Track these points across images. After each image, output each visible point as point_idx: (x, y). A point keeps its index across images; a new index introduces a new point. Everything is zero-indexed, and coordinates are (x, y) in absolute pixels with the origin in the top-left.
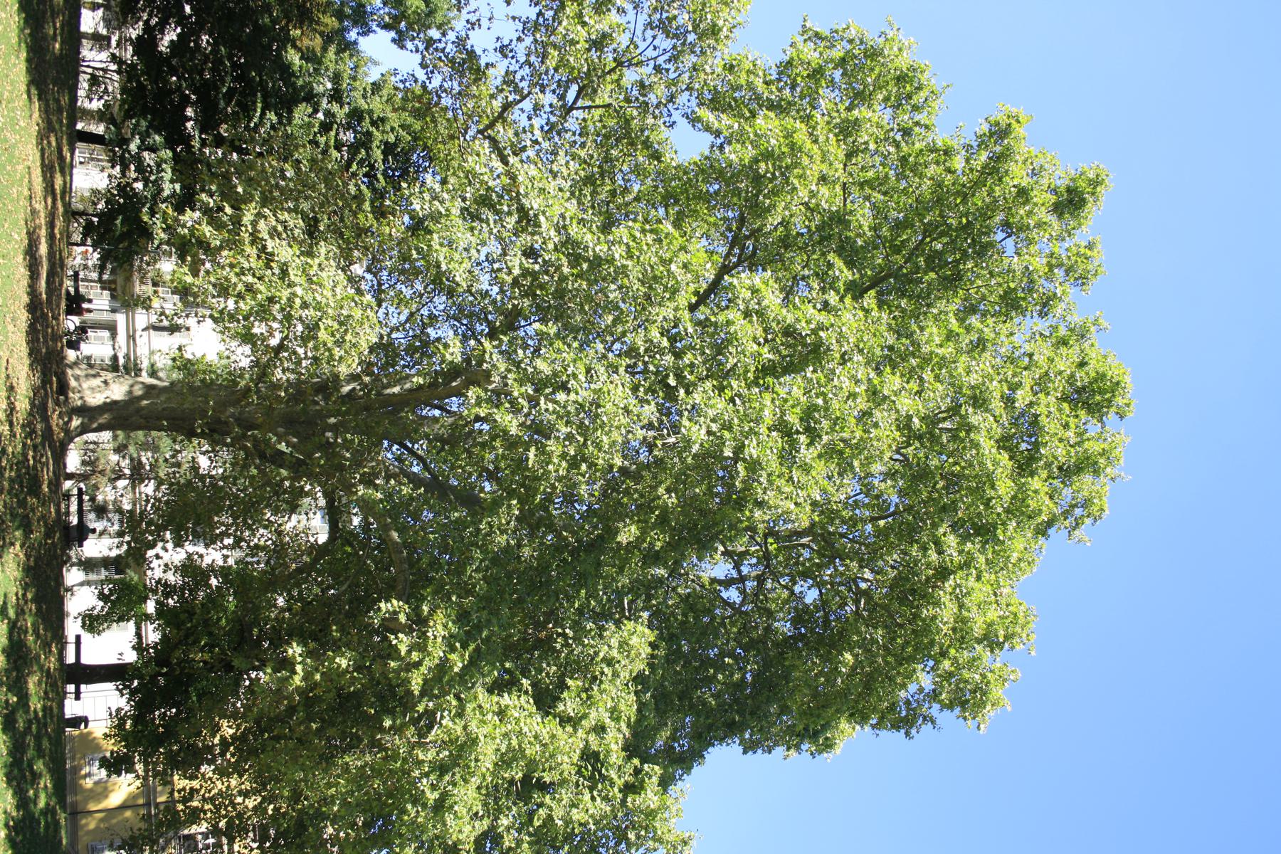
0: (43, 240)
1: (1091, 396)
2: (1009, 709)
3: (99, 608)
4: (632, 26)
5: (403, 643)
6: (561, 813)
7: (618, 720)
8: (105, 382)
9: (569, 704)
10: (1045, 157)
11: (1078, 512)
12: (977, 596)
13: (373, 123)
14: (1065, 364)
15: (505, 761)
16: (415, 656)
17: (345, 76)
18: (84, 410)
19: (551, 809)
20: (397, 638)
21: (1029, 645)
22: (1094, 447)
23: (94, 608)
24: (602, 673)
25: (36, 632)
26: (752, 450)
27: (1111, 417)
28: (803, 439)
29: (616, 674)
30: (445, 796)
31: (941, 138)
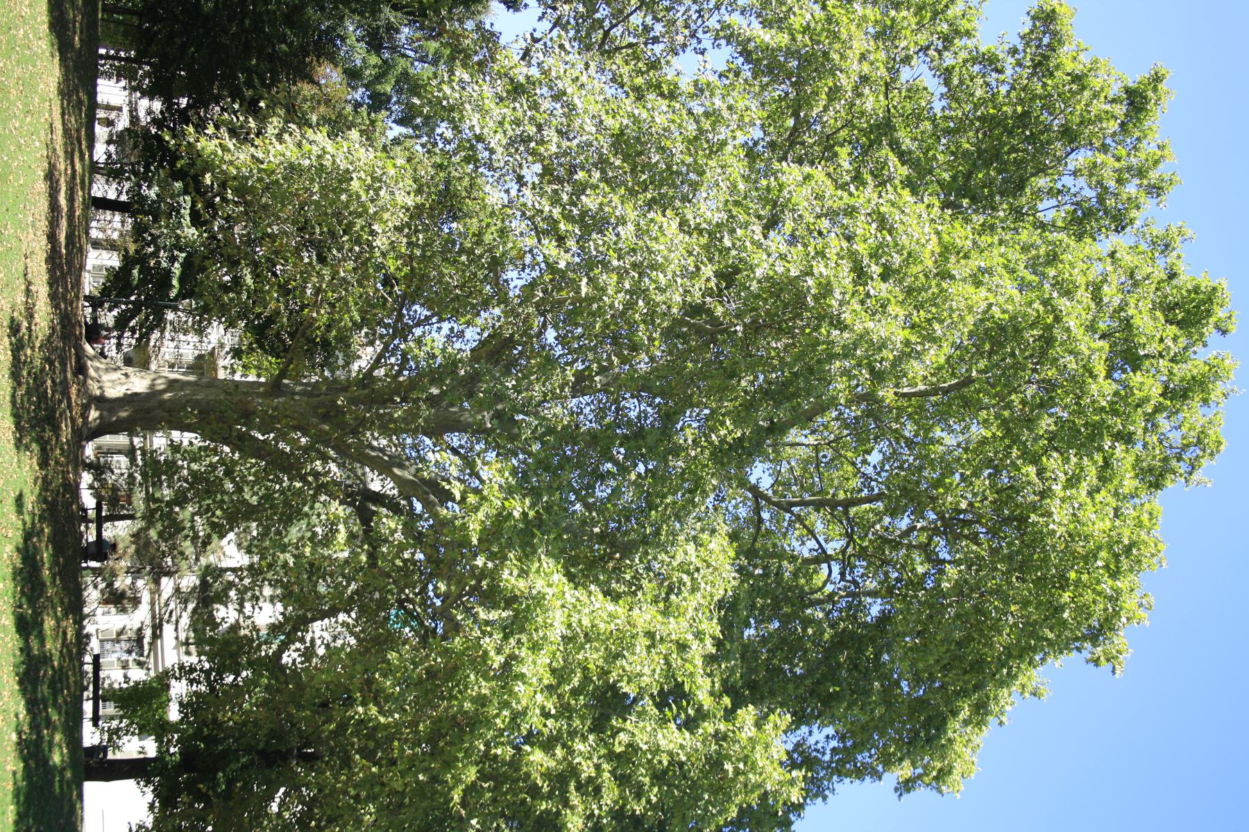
1: (1191, 313)
8: (126, 375)
10: (1104, 51)
18: (101, 401)
27: (1209, 331)
31: (985, 41)
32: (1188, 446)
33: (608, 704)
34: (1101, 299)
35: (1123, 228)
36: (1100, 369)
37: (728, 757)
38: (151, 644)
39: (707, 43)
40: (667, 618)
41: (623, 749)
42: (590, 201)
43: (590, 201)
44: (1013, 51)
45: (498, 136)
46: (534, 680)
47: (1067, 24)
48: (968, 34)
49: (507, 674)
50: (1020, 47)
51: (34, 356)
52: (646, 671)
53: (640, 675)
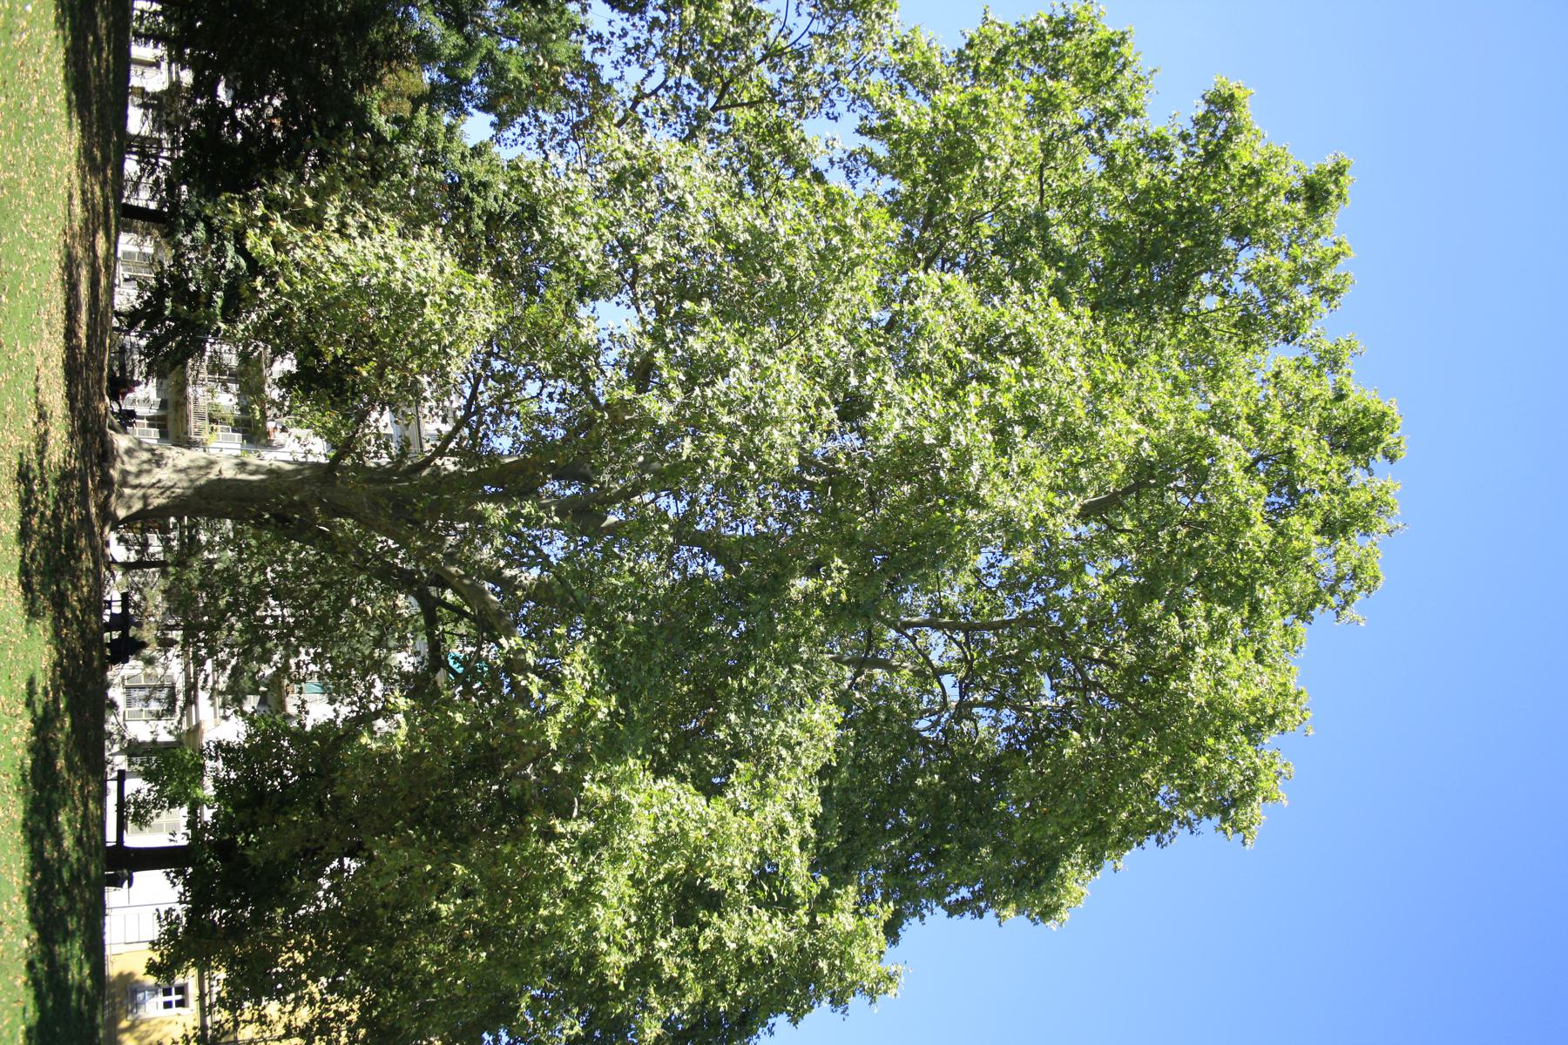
0: (84, 308)
2: (1285, 803)
3: (145, 792)
4: (782, 15)
6: (734, 935)
7: (800, 820)
9: (738, 792)
10: (1279, 143)
12: (1235, 669)
13: (473, 188)
14: (1323, 388)
15: (662, 847)
16: (551, 700)
17: (441, 136)
19: (720, 930)
20: (527, 678)
22: (1360, 498)
23: (138, 791)
24: (781, 758)
25: (68, 758)
28: (1019, 430)
29: (797, 761)
30: (589, 881)
31: (1154, 124)
32: (1343, 578)
33: (691, 899)
35: (1294, 338)
36: (1256, 511)
37: (824, 953)
38: (183, 710)
39: (841, 107)
40: (763, 817)
44: (1184, 137)
46: (615, 901)
47: (1246, 114)
48: (1135, 113)
49: (583, 898)
50: (1193, 132)
51: (47, 498)
52: (737, 862)
53: (731, 868)
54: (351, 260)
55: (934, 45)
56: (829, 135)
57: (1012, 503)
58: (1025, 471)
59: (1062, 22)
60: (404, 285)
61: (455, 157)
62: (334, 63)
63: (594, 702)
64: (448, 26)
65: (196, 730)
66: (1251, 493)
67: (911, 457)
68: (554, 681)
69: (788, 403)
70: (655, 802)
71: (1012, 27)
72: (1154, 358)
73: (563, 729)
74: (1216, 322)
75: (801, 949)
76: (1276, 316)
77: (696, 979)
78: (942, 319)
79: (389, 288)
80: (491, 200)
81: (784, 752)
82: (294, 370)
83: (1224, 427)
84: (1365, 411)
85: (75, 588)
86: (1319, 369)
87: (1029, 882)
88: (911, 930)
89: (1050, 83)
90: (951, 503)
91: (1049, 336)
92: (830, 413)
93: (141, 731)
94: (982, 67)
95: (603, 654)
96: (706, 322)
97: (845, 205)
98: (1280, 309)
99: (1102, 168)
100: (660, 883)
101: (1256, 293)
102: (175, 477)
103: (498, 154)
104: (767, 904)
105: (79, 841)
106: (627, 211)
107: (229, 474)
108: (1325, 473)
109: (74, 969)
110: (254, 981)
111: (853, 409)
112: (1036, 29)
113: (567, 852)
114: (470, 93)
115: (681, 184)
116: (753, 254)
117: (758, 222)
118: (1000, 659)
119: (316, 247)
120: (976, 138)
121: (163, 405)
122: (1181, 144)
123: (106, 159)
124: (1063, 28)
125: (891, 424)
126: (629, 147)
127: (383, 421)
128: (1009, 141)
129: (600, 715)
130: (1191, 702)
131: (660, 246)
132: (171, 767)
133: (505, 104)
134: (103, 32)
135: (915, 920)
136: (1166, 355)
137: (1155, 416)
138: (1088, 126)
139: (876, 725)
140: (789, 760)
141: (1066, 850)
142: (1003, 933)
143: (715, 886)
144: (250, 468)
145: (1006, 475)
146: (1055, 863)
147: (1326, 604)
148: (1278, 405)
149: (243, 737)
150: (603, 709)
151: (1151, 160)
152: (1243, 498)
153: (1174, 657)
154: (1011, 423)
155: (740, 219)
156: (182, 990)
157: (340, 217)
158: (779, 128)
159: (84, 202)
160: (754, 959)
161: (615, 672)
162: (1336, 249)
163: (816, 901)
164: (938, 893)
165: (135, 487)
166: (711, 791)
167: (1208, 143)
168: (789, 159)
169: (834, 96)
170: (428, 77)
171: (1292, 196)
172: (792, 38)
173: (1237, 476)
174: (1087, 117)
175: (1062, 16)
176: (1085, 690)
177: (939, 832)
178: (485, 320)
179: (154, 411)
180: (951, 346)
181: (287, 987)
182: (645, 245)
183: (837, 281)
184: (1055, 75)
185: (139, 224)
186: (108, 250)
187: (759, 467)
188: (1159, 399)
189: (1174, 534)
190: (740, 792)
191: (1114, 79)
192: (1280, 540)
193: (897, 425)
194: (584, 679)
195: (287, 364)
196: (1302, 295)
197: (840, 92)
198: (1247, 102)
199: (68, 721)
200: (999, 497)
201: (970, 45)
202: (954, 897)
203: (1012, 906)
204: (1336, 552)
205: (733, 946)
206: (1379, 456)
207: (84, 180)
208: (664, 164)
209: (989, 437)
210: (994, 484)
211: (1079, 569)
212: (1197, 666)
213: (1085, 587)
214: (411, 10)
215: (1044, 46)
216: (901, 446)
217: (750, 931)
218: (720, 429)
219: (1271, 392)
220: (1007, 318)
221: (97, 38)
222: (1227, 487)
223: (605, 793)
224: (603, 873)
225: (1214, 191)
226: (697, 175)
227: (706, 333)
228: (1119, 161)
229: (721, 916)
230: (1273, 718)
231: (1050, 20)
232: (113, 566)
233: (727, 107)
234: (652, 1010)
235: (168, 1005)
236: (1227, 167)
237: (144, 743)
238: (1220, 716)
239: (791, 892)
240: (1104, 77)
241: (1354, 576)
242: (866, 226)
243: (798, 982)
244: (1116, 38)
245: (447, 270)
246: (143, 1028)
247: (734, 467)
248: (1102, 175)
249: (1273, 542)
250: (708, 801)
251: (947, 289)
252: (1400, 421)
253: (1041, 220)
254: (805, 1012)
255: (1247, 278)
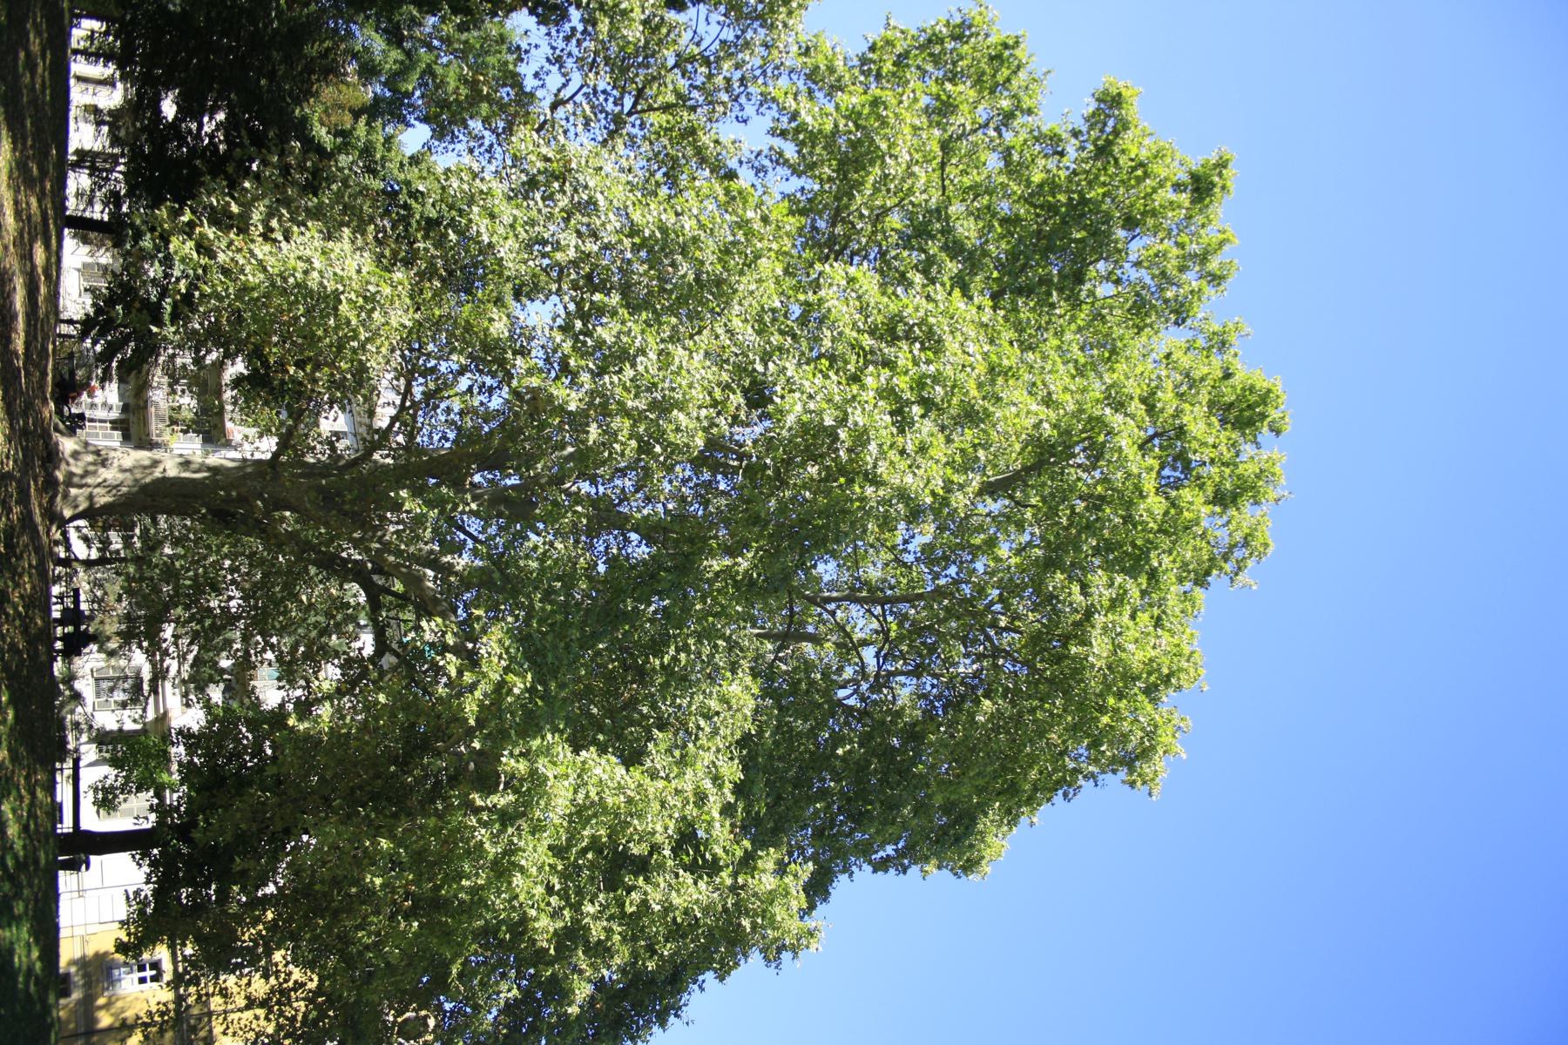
0: (21, 319)
1: (1244, 414)
2: (1184, 756)
5: (451, 663)
6: (658, 897)
7: (720, 787)
10: (1163, 138)
11: (1238, 554)
12: (1132, 634)
14: (1211, 367)
15: (580, 814)
16: (468, 677)
17: (379, 146)
19: (645, 893)
21: (1199, 679)
22: (1248, 469)
24: (699, 728)
26: (857, 417)
28: (916, 410)
30: (511, 850)
31: (1048, 121)
32: (1235, 546)
33: (617, 865)
34: (1154, 406)
36: (1149, 484)
39: (750, 110)
40: (686, 780)
41: (634, 909)
42: (606, 332)
43: (606, 332)
45: (510, 242)
48: (1029, 112)
49: (503, 868)
50: (1084, 129)
52: (659, 828)
53: (654, 833)
54: (271, 261)
55: (838, 50)
56: (743, 135)
57: (909, 479)
58: (923, 449)
59: (959, 26)
60: (321, 284)
61: (393, 166)
62: (271, 76)
63: (511, 678)
64: (389, 42)
65: (163, 718)
66: (1143, 467)
67: (815, 439)
68: (472, 660)
69: (691, 386)
70: (572, 776)
71: (914, 32)
72: (1056, 342)
73: (481, 705)
74: (1111, 308)
75: (725, 910)
76: (1166, 301)
77: (624, 939)
78: (845, 309)
79: (306, 287)
80: (429, 206)
81: (702, 723)
82: (246, 372)
83: (1119, 406)
84: (1252, 389)
85: (17, 585)
86: (1209, 349)
87: (949, 839)
88: (841, 886)
89: (948, 86)
90: (850, 481)
91: (950, 325)
92: (737, 399)
93: (108, 720)
94: (885, 70)
95: (522, 638)
96: (614, 313)
97: (745, 202)
98: (1169, 294)
99: (1002, 164)
100: (584, 851)
101: (1148, 280)
102: (121, 476)
103: (435, 163)
104: (692, 868)
105: (25, 828)
106: (539, 211)
107: (173, 472)
108: (1214, 446)
109: (20, 950)
110: (220, 954)
111: (758, 396)
112: (934, 34)
113: (485, 825)
114: (410, 105)
115: (591, 184)
116: (660, 248)
117: (663, 217)
118: (918, 630)
119: (239, 250)
120: (877, 139)
121: (125, 408)
122: (1073, 141)
123: (43, 173)
124: (961, 32)
125: (794, 410)
126: (544, 150)
127: (333, 422)
128: (907, 141)
129: (516, 691)
130: (1093, 666)
131: (573, 243)
132: (135, 754)
133: (446, 119)
134: (35, 47)
135: (843, 878)
136: (1067, 336)
137: (1054, 397)
138: (986, 125)
139: (790, 694)
140: (708, 730)
141: (982, 809)
142: (928, 886)
143: (636, 851)
144: (193, 466)
145: (902, 452)
146: (974, 821)
147: (1221, 569)
148: (1169, 385)
149: (203, 723)
150: (518, 685)
151: (1046, 156)
152: (1135, 471)
153: (1076, 624)
154: (909, 403)
155: (648, 217)
156: (156, 965)
157: (266, 223)
158: (692, 131)
159: (18, 214)
160: (679, 920)
161: (531, 650)
162: (1221, 237)
163: (740, 862)
164: (865, 851)
165: (80, 486)
166: (632, 758)
167: (1098, 138)
168: (703, 160)
169: (743, 100)
170: (368, 93)
171: (1177, 187)
172: (704, 45)
173: (1131, 452)
174: (985, 117)
175: (958, 21)
176: (995, 657)
177: (862, 794)
178: (401, 317)
179: (115, 414)
180: (854, 334)
181: (255, 958)
182: (558, 242)
183: (742, 273)
184: (953, 78)
185: (92, 235)
186: (48, 259)
187: (665, 450)
188: (1060, 381)
189: (1072, 508)
190: (657, 758)
191: (1008, 80)
192: (1173, 511)
193: (798, 408)
194: (500, 657)
195: (238, 367)
196: (1191, 280)
197: (749, 96)
198: (1135, 100)
199: (11, 715)
200: (895, 473)
201: (872, 49)
202: (882, 854)
203: (934, 861)
204: (1229, 522)
205: (657, 908)
206: (1265, 429)
207: (17, 191)
208: (574, 165)
209: (888, 418)
210: (892, 462)
211: (991, 543)
212: (1096, 632)
213: (998, 560)
214: (354, 27)
215: (941, 49)
216: (804, 428)
217: (674, 894)
218: (627, 413)
219: (1164, 373)
220: (910, 310)
221: (28, 55)
222: (1123, 460)
223: (522, 767)
224: (522, 844)
225: (1104, 184)
226: (610, 175)
227: (616, 327)
228: (1016, 157)
229: (647, 880)
230: (1168, 676)
231: (948, 24)
232: (75, 564)
233: (643, 111)
234: (581, 972)
235: (142, 980)
236: (1116, 160)
237: (111, 732)
238: (1121, 678)
239: (714, 856)
240: (1000, 78)
241: (1246, 544)
242: (765, 220)
243: (721, 942)
244: (1011, 42)
245: (365, 270)
246: (119, 1004)
247: (640, 450)
248: (1000, 172)
249: (1166, 513)
250: (628, 770)
251: (851, 280)
252: (1284, 397)
253: (939, 212)
254: (731, 968)
255: (1138, 264)
